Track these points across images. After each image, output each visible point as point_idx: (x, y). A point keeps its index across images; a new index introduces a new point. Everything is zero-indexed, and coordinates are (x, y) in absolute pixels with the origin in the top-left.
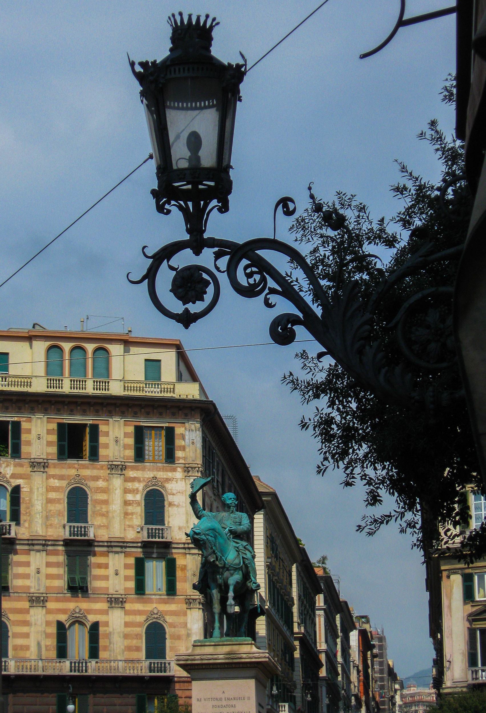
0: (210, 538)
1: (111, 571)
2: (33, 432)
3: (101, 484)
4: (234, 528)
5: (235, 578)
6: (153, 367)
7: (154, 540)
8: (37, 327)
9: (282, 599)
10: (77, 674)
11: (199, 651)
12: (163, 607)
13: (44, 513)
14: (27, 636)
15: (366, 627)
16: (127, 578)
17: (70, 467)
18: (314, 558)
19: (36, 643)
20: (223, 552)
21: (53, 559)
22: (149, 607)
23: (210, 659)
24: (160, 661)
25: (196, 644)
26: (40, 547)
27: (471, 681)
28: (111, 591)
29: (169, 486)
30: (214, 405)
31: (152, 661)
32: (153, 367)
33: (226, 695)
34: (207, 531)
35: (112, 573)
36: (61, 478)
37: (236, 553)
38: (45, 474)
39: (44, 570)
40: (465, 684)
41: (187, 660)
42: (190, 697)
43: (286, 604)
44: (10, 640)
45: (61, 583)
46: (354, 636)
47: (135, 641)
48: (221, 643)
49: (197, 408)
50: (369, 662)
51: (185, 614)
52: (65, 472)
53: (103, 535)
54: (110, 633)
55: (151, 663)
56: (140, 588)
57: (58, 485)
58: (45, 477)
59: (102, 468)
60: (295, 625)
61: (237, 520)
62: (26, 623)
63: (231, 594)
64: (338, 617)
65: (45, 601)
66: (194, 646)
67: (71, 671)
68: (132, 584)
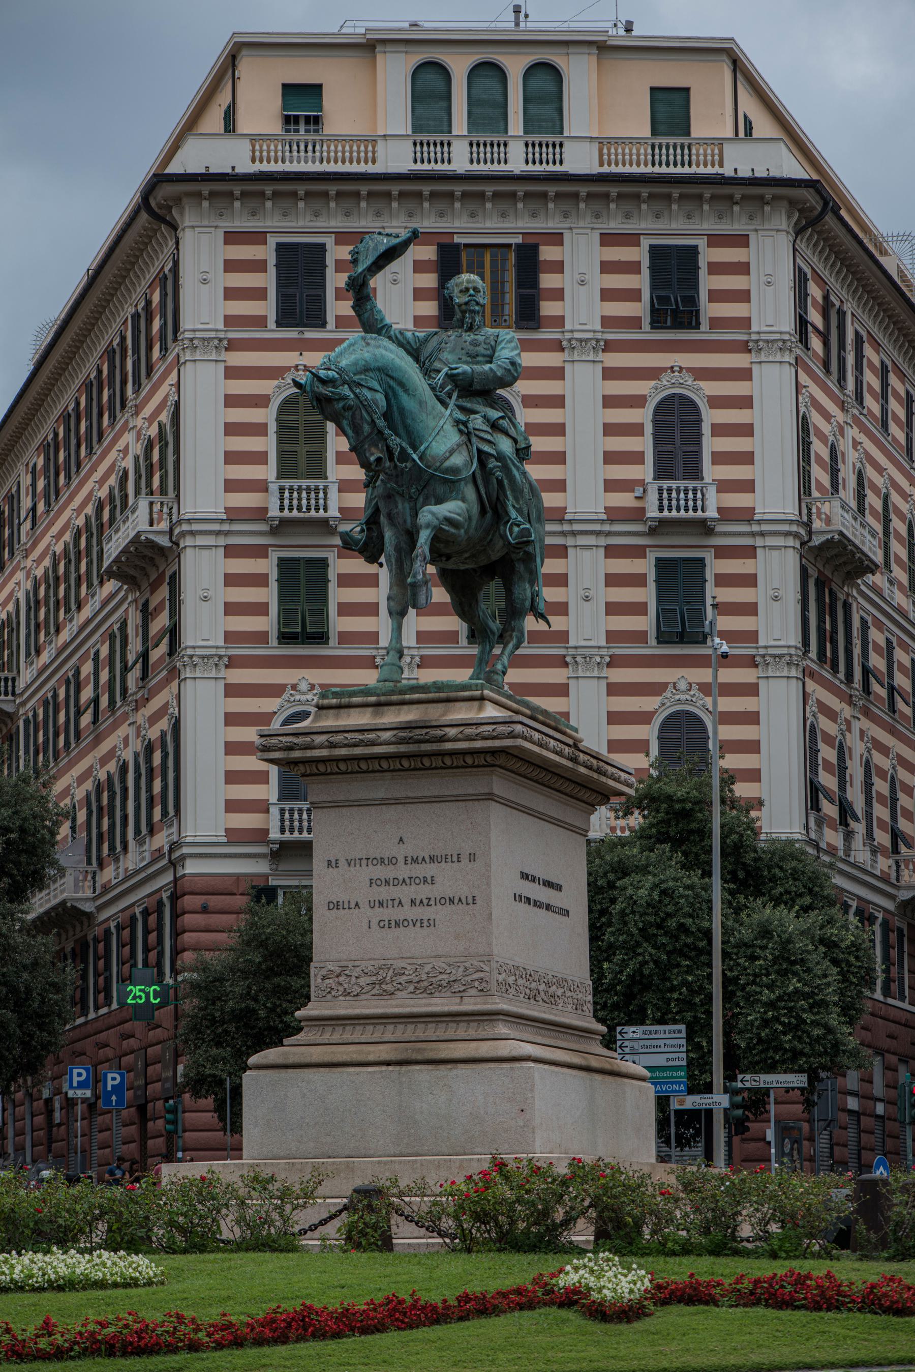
0: (368, 394)
6: (671, 110)
23: (355, 745)
25: (326, 702)
32: (671, 110)
33: (409, 849)
34: (360, 373)
41: (290, 748)
48: (394, 698)
61: (481, 349)
66: (320, 708)
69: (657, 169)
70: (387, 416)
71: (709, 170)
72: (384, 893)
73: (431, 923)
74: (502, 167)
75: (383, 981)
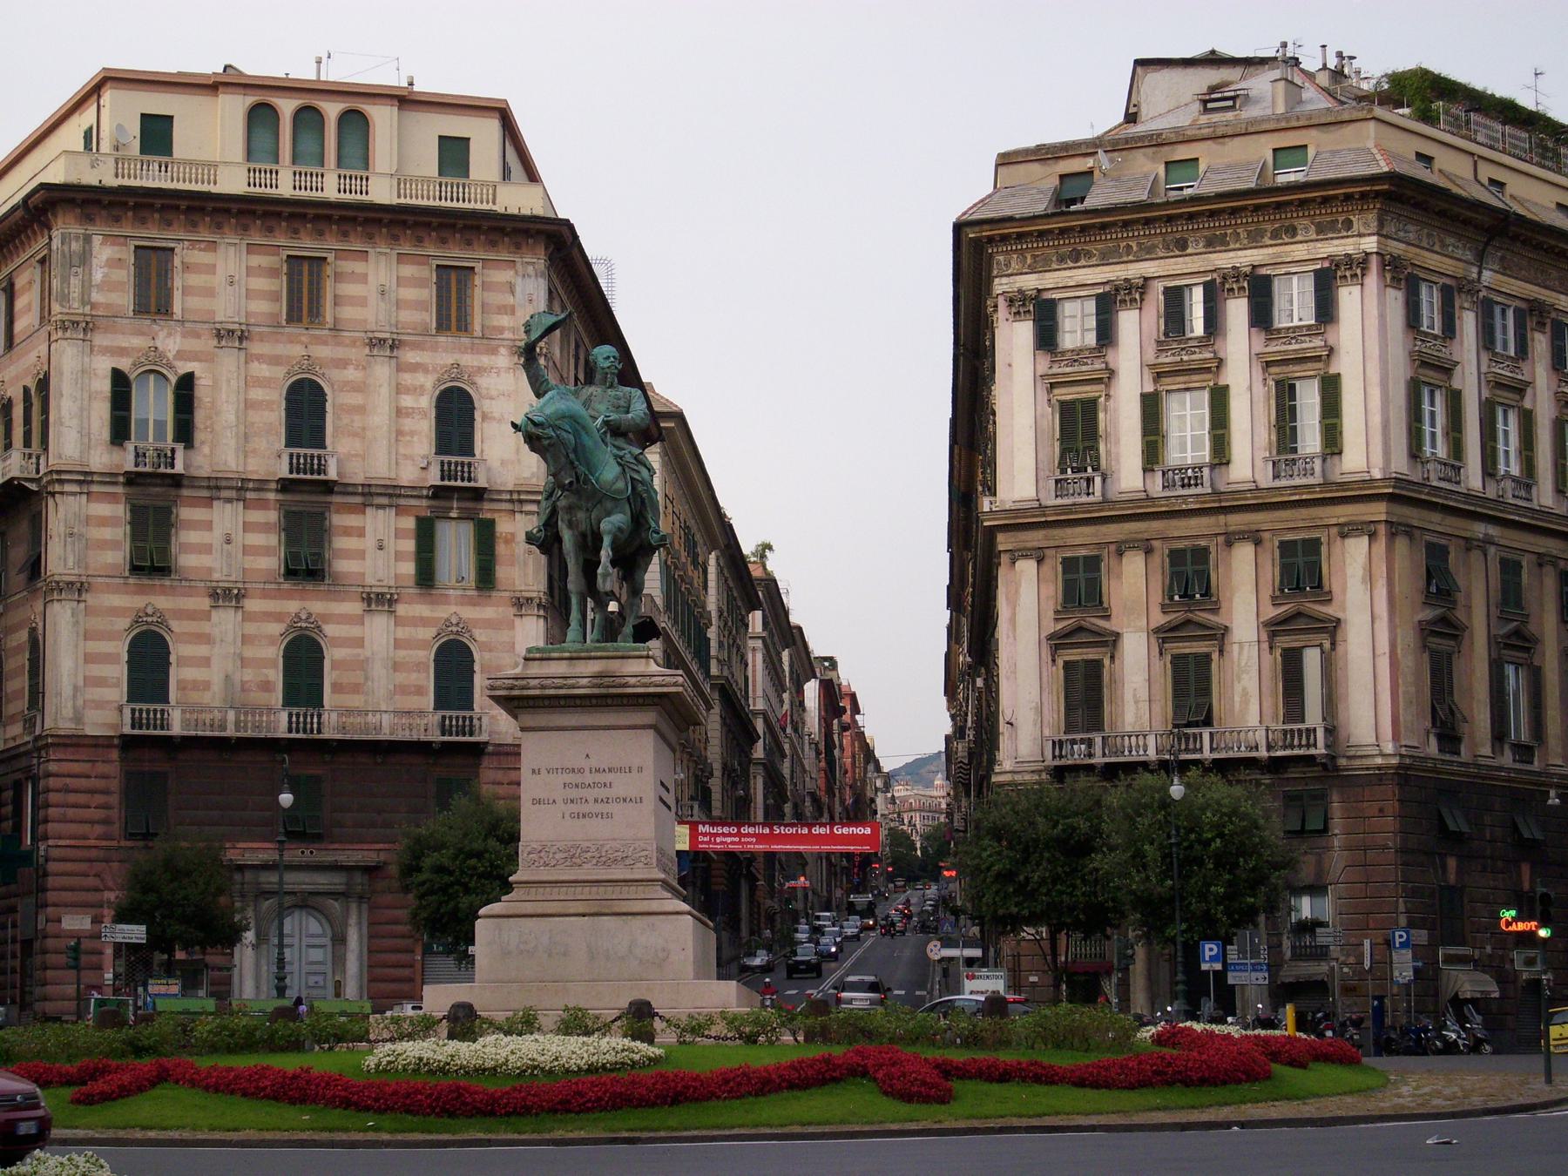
0: (564, 434)
1: (369, 543)
2: (220, 270)
3: (351, 374)
4: (614, 416)
5: (614, 522)
6: (454, 153)
7: (452, 483)
8: (229, 71)
9: (691, 613)
10: (301, 735)
11: (536, 669)
12: (468, 613)
13: (242, 428)
14: (206, 662)
15: (830, 675)
16: (399, 556)
17: (291, 340)
18: (747, 547)
19: (222, 676)
20: (591, 468)
21: (257, 516)
22: (443, 612)
24: (461, 713)
26: (233, 494)
27: (1050, 762)
28: (369, 580)
29: (483, 382)
30: (571, 227)
31: (448, 713)
32: (454, 153)
33: (594, 762)
35: (372, 547)
36: (275, 360)
37: (618, 469)
38: (243, 353)
39: (239, 538)
40: (1040, 766)
42: (519, 784)
43: (697, 623)
44: (172, 671)
45: (271, 563)
46: (811, 689)
47: (414, 676)
49: (539, 232)
50: (836, 737)
51: (512, 626)
52: (282, 349)
53: (357, 474)
54: (367, 659)
55: (444, 718)
56: (426, 577)
57: (267, 374)
58: (242, 360)
59: (354, 343)
60: (713, 663)
61: (622, 403)
62: (206, 639)
63: (605, 554)
64: (785, 655)
65: (240, 597)
66: (526, 659)
67: (290, 731)
68: (409, 568)
69: (443, 203)
70: (575, 451)
71: (485, 207)
72: (574, 793)
73: (609, 816)
74: (319, 194)
75: (573, 856)
